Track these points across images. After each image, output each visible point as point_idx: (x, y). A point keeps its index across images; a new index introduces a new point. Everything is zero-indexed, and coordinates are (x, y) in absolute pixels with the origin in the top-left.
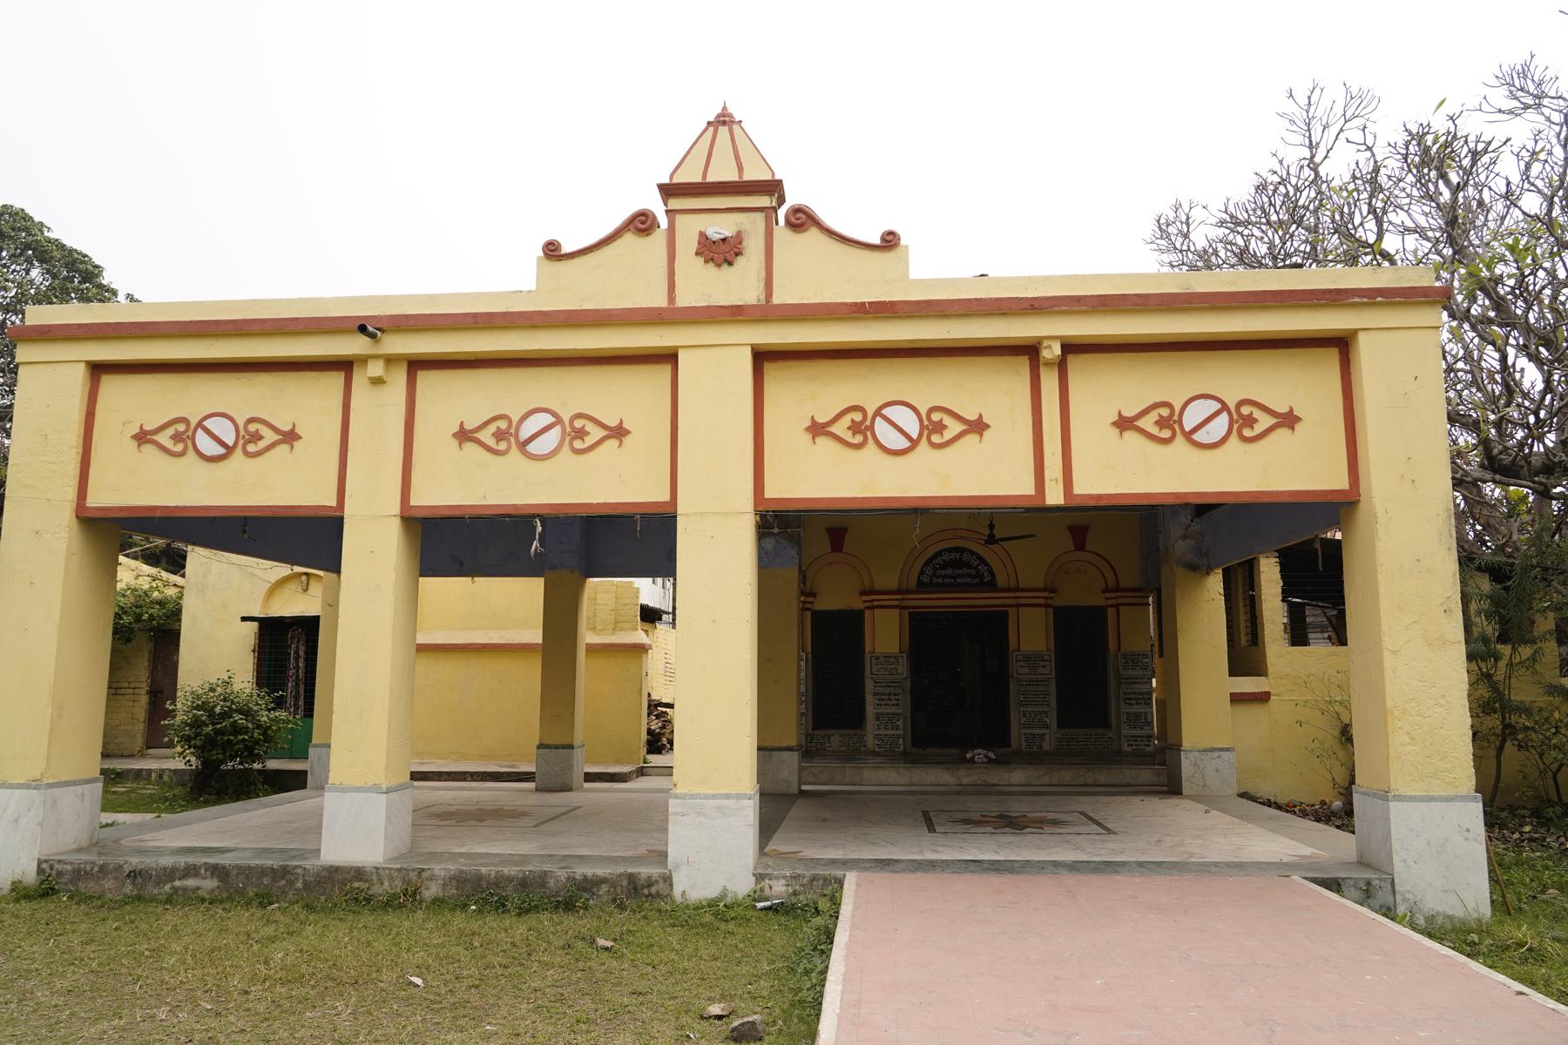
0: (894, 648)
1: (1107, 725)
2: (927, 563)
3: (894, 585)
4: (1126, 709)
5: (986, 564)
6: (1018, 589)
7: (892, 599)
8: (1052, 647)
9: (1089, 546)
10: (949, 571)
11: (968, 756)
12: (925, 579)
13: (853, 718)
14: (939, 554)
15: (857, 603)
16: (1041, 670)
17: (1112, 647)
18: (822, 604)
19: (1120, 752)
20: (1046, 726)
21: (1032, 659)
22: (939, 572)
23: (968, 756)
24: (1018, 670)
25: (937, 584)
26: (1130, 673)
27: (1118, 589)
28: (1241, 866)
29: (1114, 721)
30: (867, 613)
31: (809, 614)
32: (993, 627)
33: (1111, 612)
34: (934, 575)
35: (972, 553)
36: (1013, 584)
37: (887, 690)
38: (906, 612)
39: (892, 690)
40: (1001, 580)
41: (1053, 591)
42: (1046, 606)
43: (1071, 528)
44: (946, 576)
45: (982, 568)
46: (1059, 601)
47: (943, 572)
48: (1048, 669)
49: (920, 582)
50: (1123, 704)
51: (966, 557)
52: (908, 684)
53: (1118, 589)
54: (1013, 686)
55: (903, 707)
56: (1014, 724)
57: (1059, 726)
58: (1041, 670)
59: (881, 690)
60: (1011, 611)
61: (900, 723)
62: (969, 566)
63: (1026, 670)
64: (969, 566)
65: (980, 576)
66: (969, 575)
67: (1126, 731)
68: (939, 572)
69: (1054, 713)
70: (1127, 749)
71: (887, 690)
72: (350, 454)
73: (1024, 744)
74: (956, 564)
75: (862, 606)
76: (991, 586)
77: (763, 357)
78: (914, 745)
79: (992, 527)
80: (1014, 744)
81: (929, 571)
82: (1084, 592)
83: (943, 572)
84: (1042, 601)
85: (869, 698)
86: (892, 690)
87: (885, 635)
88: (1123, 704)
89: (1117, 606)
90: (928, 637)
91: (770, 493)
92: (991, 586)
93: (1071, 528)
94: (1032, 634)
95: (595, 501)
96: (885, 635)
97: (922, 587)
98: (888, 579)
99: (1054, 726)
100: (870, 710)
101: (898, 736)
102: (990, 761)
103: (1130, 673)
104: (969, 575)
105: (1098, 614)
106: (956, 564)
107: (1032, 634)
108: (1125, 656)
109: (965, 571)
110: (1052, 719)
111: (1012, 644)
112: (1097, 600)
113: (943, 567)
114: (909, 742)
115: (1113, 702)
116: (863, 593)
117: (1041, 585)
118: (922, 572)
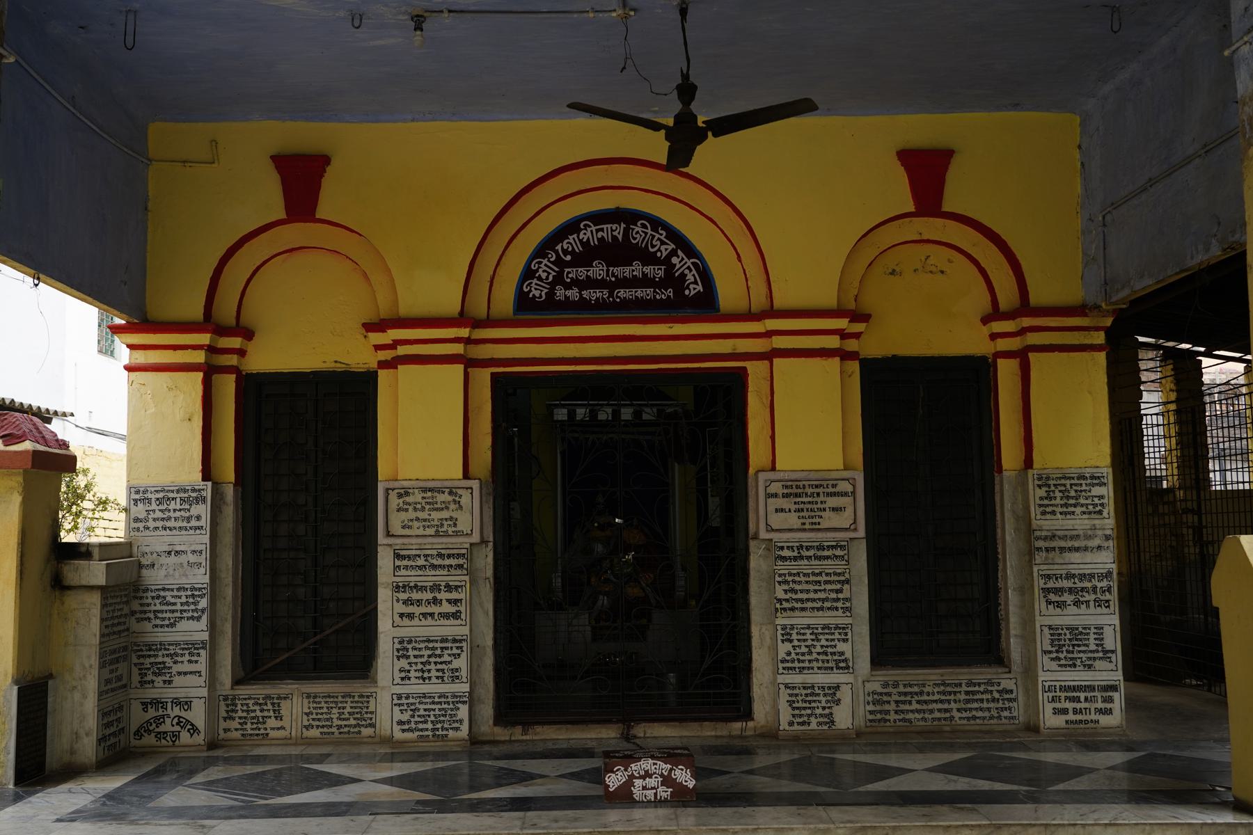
1: (990, 650)
2: (541, 251)
3: (451, 305)
4: (1047, 617)
5: (691, 251)
6: (772, 312)
7: (447, 340)
9: (950, 203)
10: (598, 270)
11: (614, 780)
12: (537, 291)
13: (343, 649)
14: (571, 227)
16: (830, 520)
17: (1010, 455)
18: (272, 355)
19: (1032, 728)
20: (843, 665)
21: (806, 492)
22: (572, 273)
23: (614, 780)
24: (771, 519)
25: (567, 305)
27: (1025, 308)
28: (396, 402)
30: (382, 374)
31: (227, 387)
32: (712, 409)
33: (1007, 371)
34: (559, 280)
35: (656, 223)
36: (759, 301)
37: (429, 578)
38: (483, 377)
39: (441, 577)
40: (729, 293)
42: (845, 356)
44: (591, 283)
46: (876, 345)
47: (581, 273)
48: (848, 517)
49: (524, 302)
50: (1040, 604)
51: (639, 233)
52: (486, 561)
53: (1025, 308)
54: (757, 563)
55: (472, 622)
57: (878, 661)
58: (830, 520)
59: (413, 577)
60: (756, 370)
61: (462, 663)
62: (649, 259)
63: (793, 520)
64: (649, 259)
65: (674, 281)
66: (645, 282)
67: (1049, 674)
68: (572, 273)
69: (863, 631)
70: (1051, 721)
71: (429, 578)
73: (785, 715)
75: (373, 365)
76: (705, 304)
78: (501, 718)
79: (687, 91)
80: (761, 710)
81: (545, 269)
82: (937, 320)
83: (581, 273)
84: (833, 342)
85: (384, 596)
86: (441, 577)
87: (426, 435)
88: (1040, 604)
89: (1022, 356)
90: (522, 416)
91: (282, 215)
92: (705, 304)
94: (806, 429)
96: (426, 435)
100: (387, 630)
104: (645, 282)
105: (973, 376)
107: (806, 429)
108: (1044, 481)
110: (859, 646)
111: (757, 453)
112: (967, 339)
113: (585, 256)
114: (487, 711)
116: (370, 327)
117: (830, 301)
118: (528, 274)
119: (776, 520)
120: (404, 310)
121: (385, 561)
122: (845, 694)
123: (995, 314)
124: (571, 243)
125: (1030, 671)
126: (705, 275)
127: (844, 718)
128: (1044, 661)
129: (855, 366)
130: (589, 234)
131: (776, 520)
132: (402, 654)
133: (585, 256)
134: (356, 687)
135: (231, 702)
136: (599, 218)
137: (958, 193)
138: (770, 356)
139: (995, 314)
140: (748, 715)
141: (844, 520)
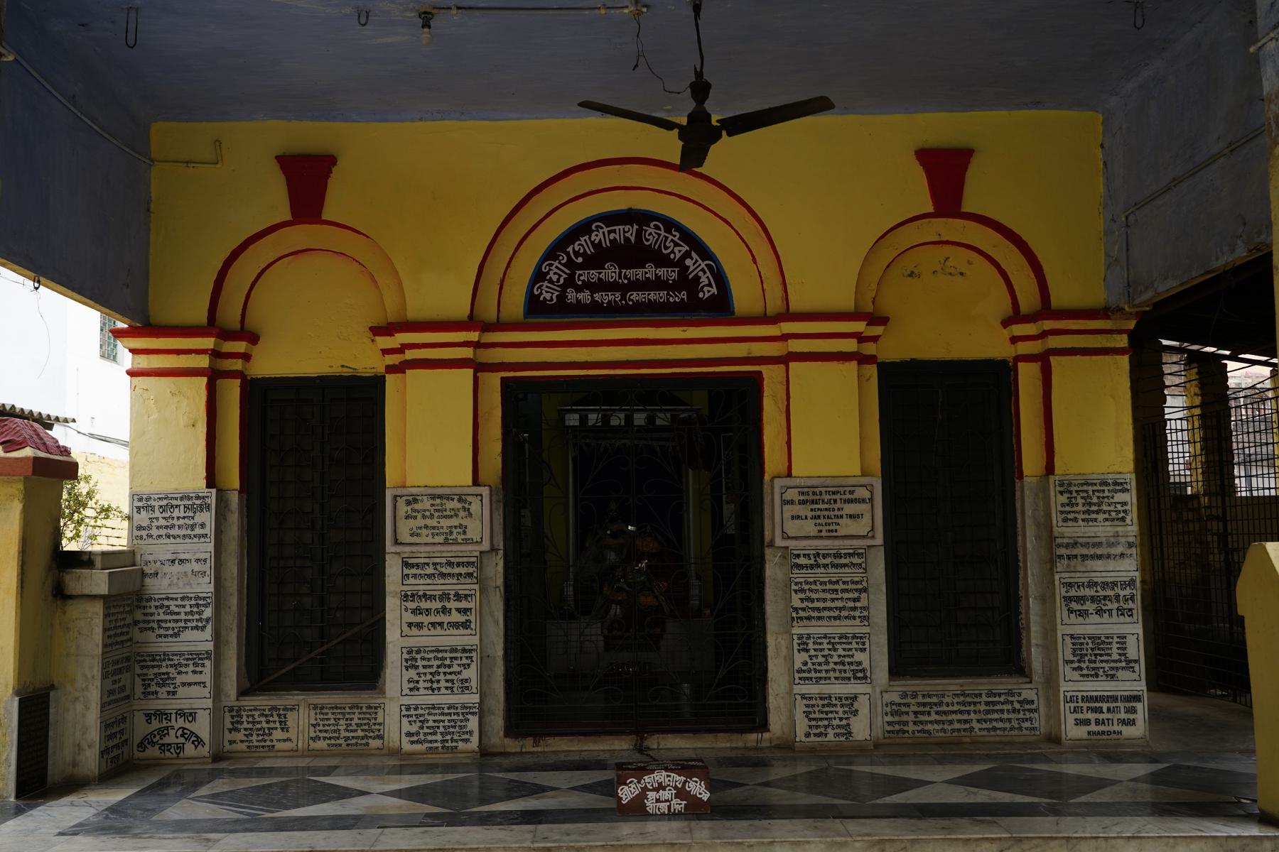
0: (453, 469)
1: (1014, 664)
2: (552, 253)
3: (461, 309)
4: (1068, 626)
5: (705, 253)
6: (788, 315)
7: (457, 344)
10: (610, 272)
11: (627, 793)
12: (548, 294)
13: (350, 659)
14: (583, 228)
15: (365, 358)
16: (847, 527)
17: (1031, 462)
20: (861, 675)
21: (823, 498)
22: (583, 276)
23: (627, 793)
24: (787, 526)
25: (579, 308)
26: (1080, 530)
27: (1046, 310)
29: (1036, 659)
31: (232, 392)
32: (727, 413)
33: (1028, 375)
34: (570, 282)
35: (670, 224)
36: (774, 304)
37: (439, 586)
38: (493, 382)
39: (450, 586)
40: (744, 296)
41: (876, 319)
42: (862, 359)
45: (694, 264)
46: (894, 348)
47: (594, 275)
48: (865, 524)
49: (534, 305)
50: (1061, 613)
51: (652, 235)
52: (496, 569)
54: (773, 570)
55: (481, 631)
56: (776, 669)
57: (896, 670)
58: (847, 527)
59: (421, 586)
60: (771, 374)
61: (472, 673)
62: (663, 261)
63: (810, 527)
64: (663, 261)
66: (659, 284)
67: (1071, 684)
68: (583, 276)
69: (881, 640)
70: (1072, 731)
71: (439, 586)
73: (802, 726)
74: (632, 254)
76: (720, 307)
77: (789, 475)
78: (512, 729)
79: (700, 89)
80: (777, 722)
81: (556, 271)
82: (956, 323)
83: (594, 275)
84: (850, 345)
85: (392, 606)
86: (450, 586)
87: (435, 441)
88: (1061, 613)
89: (1043, 359)
90: (536, 429)
92: (720, 307)
94: (823, 434)
95: (1251, 672)
96: (435, 441)
98: (447, 294)
99: (881, 673)
100: (395, 640)
101: (467, 709)
102: (695, 811)
103: (1080, 530)
104: (659, 284)
105: (998, 377)
106: (632, 254)
107: (823, 434)
108: (1065, 487)
109: (650, 271)
110: (876, 656)
111: (773, 460)
113: (597, 259)
114: (497, 722)
118: (539, 276)
119: (793, 528)
120: (413, 314)
121: (393, 570)
122: (863, 705)
124: (583, 244)
125: (1051, 681)
126: (720, 278)
127: (861, 729)
128: (1066, 671)
129: (872, 370)
130: (601, 235)
131: (793, 528)
132: (410, 664)
133: (597, 259)
134: (364, 698)
135: (236, 712)
136: (611, 219)
137: (979, 193)
141: (862, 527)
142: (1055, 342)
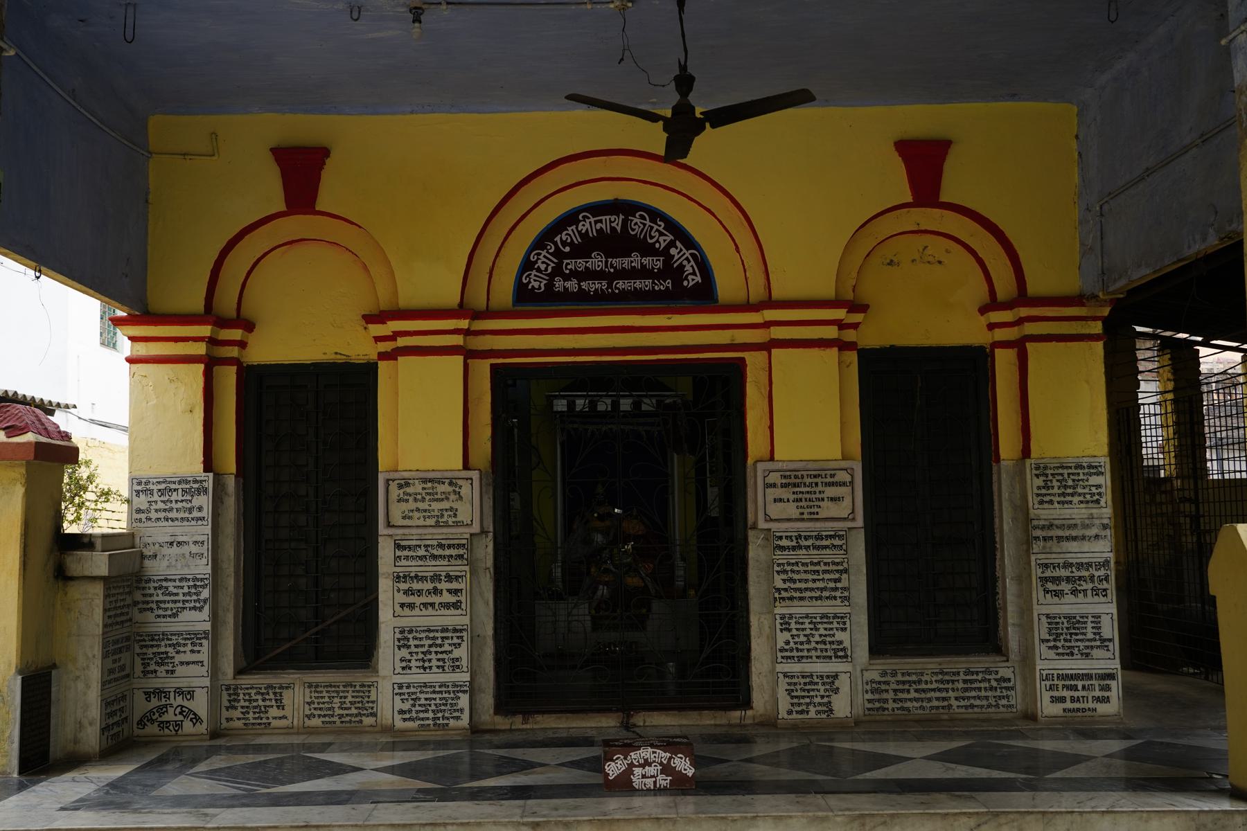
2: (539, 244)
3: (451, 297)
4: (1044, 606)
5: (689, 242)
6: (770, 303)
7: (446, 332)
8: (856, 449)
9: (948, 194)
10: (596, 261)
11: (614, 769)
12: (536, 282)
15: (358, 345)
16: (828, 509)
17: (1008, 445)
18: (269, 348)
19: (1030, 716)
20: (842, 654)
21: (804, 482)
22: (570, 265)
23: (614, 769)
24: (769, 509)
25: (566, 296)
27: (1022, 297)
30: (383, 366)
31: (228, 378)
32: (710, 400)
33: (1004, 361)
34: (558, 271)
35: (655, 215)
36: (757, 292)
37: (430, 568)
38: (482, 369)
39: (442, 567)
40: (727, 285)
42: (843, 346)
43: (905, 148)
46: (874, 335)
47: (580, 264)
48: (846, 507)
49: (523, 293)
50: (1037, 593)
51: (638, 224)
52: (486, 551)
53: (1022, 297)
54: (756, 552)
55: (471, 612)
56: (759, 648)
57: (876, 650)
58: (828, 509)
59: (413, 567)
60: (754, 361)
61: (462, 653)
63: (792, 510)
66: (644, 273)
67: (1047, 662)
68: (570, 265)
70: (1048, 709)
71: (430, 568)
72: (461, 428)
73: (784, 703)
76: (703, 295)
79: (684, 82)
80: (760, 700)
81: (544, 261)
82: (935, 310)
83: (580, 264)
84: (831, 332)
85: (385, 586)
86: (442, 567)
87: (426, 426)
88: (1037, 593)
90: (524, 413)
92: (703, 295)
93: (905, 148)
94: (804, 419)
96: (426, 426)
97: (527, 299)
100: (388, 620)
102: (680, 786)
104: (644, 273)
105: (974, 363)
107: (804, 419)
108: (1041, 471)
109: (635, 260)
110: (857, 636)
111: (756, 444)
113: (583, 249)
114: (487, 700)
115: (1010, 591)
116: (370, 319)
117: (829, 292)
118: (527, 265)
119: (775, 510)
120: (404, 302)
121: (385, 552)
122: (843, 683)
123: (992, 304)
125: (1027, 660)
126: (704, 267)
127: (842, 707)
128: (1042, 650)
129: (853, 357)
130: (587, 225)
131: (775, 510)
132: (403, 644)
133: (583, 249)
134: (358, 677)
135: (233, 691)
138: (768, 346)
139: (992, 304)
140: (747, 704)
141: (842, 510)
142: (1031, 329)
